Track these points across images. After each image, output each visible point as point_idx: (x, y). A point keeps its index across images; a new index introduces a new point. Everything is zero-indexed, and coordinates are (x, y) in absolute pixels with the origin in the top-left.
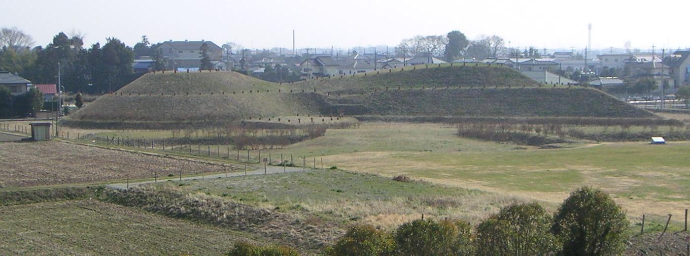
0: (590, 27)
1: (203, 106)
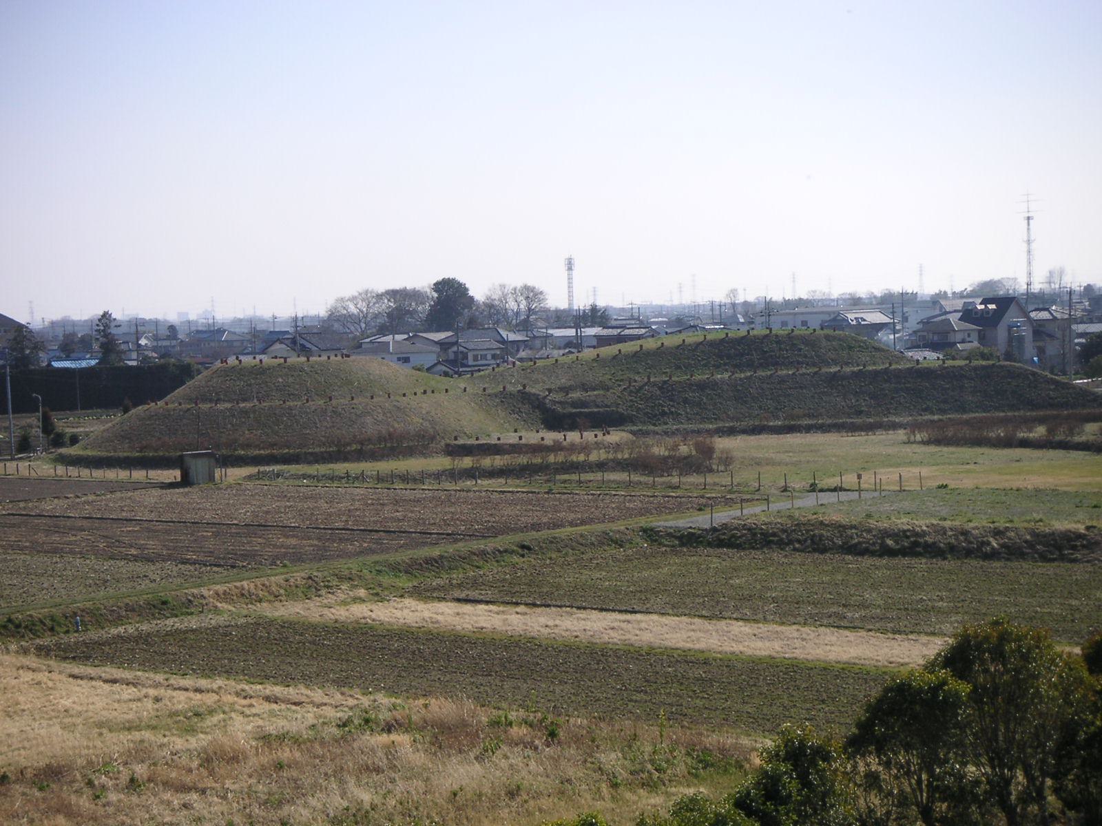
0: (570, 266)
1: (369, 420)
